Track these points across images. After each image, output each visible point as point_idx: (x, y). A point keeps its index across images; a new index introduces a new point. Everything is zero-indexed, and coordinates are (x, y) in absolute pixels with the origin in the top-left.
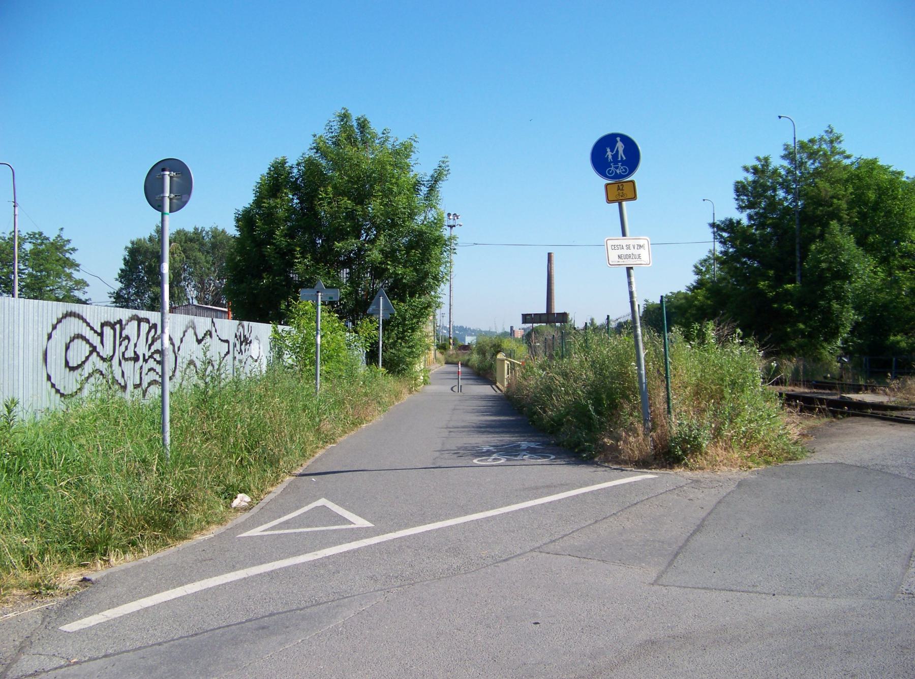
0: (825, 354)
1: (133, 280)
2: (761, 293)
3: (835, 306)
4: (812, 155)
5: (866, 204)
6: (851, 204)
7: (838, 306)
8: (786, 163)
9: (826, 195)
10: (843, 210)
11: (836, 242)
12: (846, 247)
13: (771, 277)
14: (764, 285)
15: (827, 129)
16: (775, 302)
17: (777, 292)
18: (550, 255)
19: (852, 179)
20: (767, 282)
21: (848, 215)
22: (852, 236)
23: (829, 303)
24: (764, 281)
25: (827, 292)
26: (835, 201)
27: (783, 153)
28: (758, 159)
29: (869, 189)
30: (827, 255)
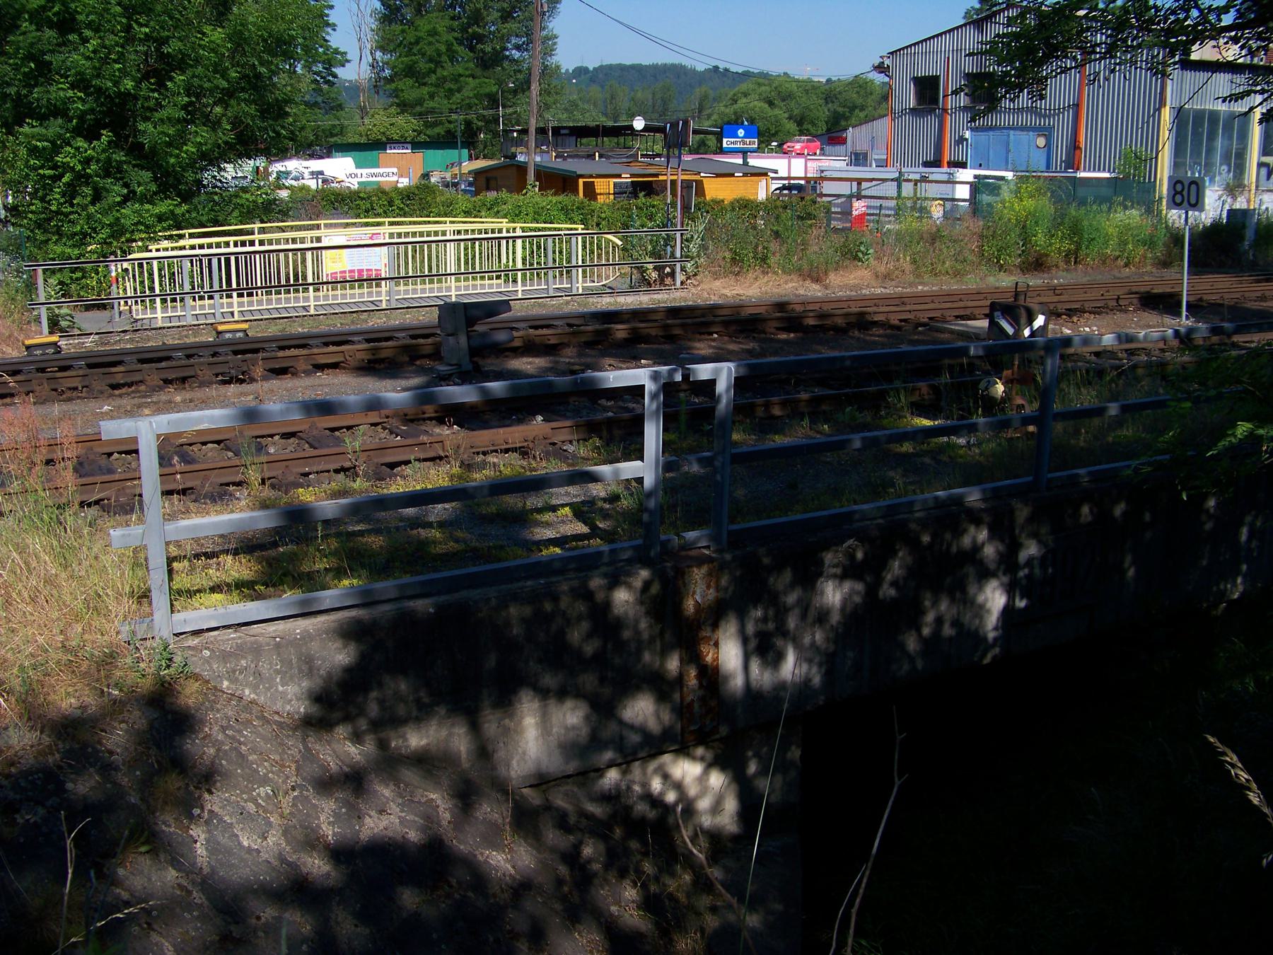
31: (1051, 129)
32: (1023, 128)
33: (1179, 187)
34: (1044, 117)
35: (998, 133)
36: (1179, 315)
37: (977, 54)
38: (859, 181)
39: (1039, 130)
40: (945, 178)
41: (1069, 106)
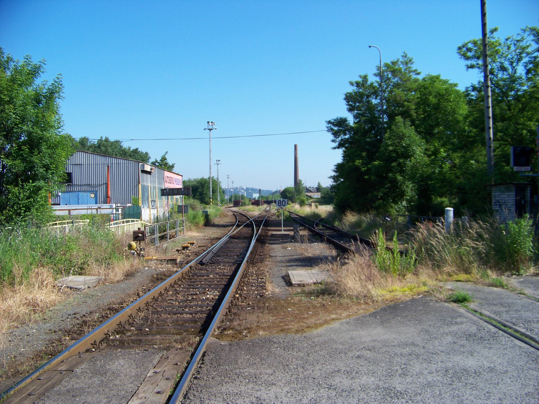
0: (393, 212)
1: (403, 147)
2: (357, 168)
3: (399, 178)
4: (394, 72)
5: (429, 106)
6: (418, 105)
7: (401, 178)
8: (378, 79)
9: (400, 99)
10: (412, 110)
11: (400, 131)
12: (407, 135)
13: (364, 157)
14: (359, 163)
15: (403, 54)
16: (367, 175)
17: (368, 167)
18: (295, 146)
19: (420, 88)
20: (361, 161)
21: (416, 113)
22: (413, 127)
23: (395, 175)
24: (359, 159)
25: (394, 167)
26: (406, 103)
27: (376, 72)
28: (360, 77)
29: (430, 95)
30: (393, 141)
31: (97, 191)
32: (84, 191)
33: (280, 202)
34: (94, 187)
35: (74, 193)
36: (281, 227)
37: (78, 164)
38: (69, 210)
39: (91, 192)
40: (109, 207)
41: (103, 184)
